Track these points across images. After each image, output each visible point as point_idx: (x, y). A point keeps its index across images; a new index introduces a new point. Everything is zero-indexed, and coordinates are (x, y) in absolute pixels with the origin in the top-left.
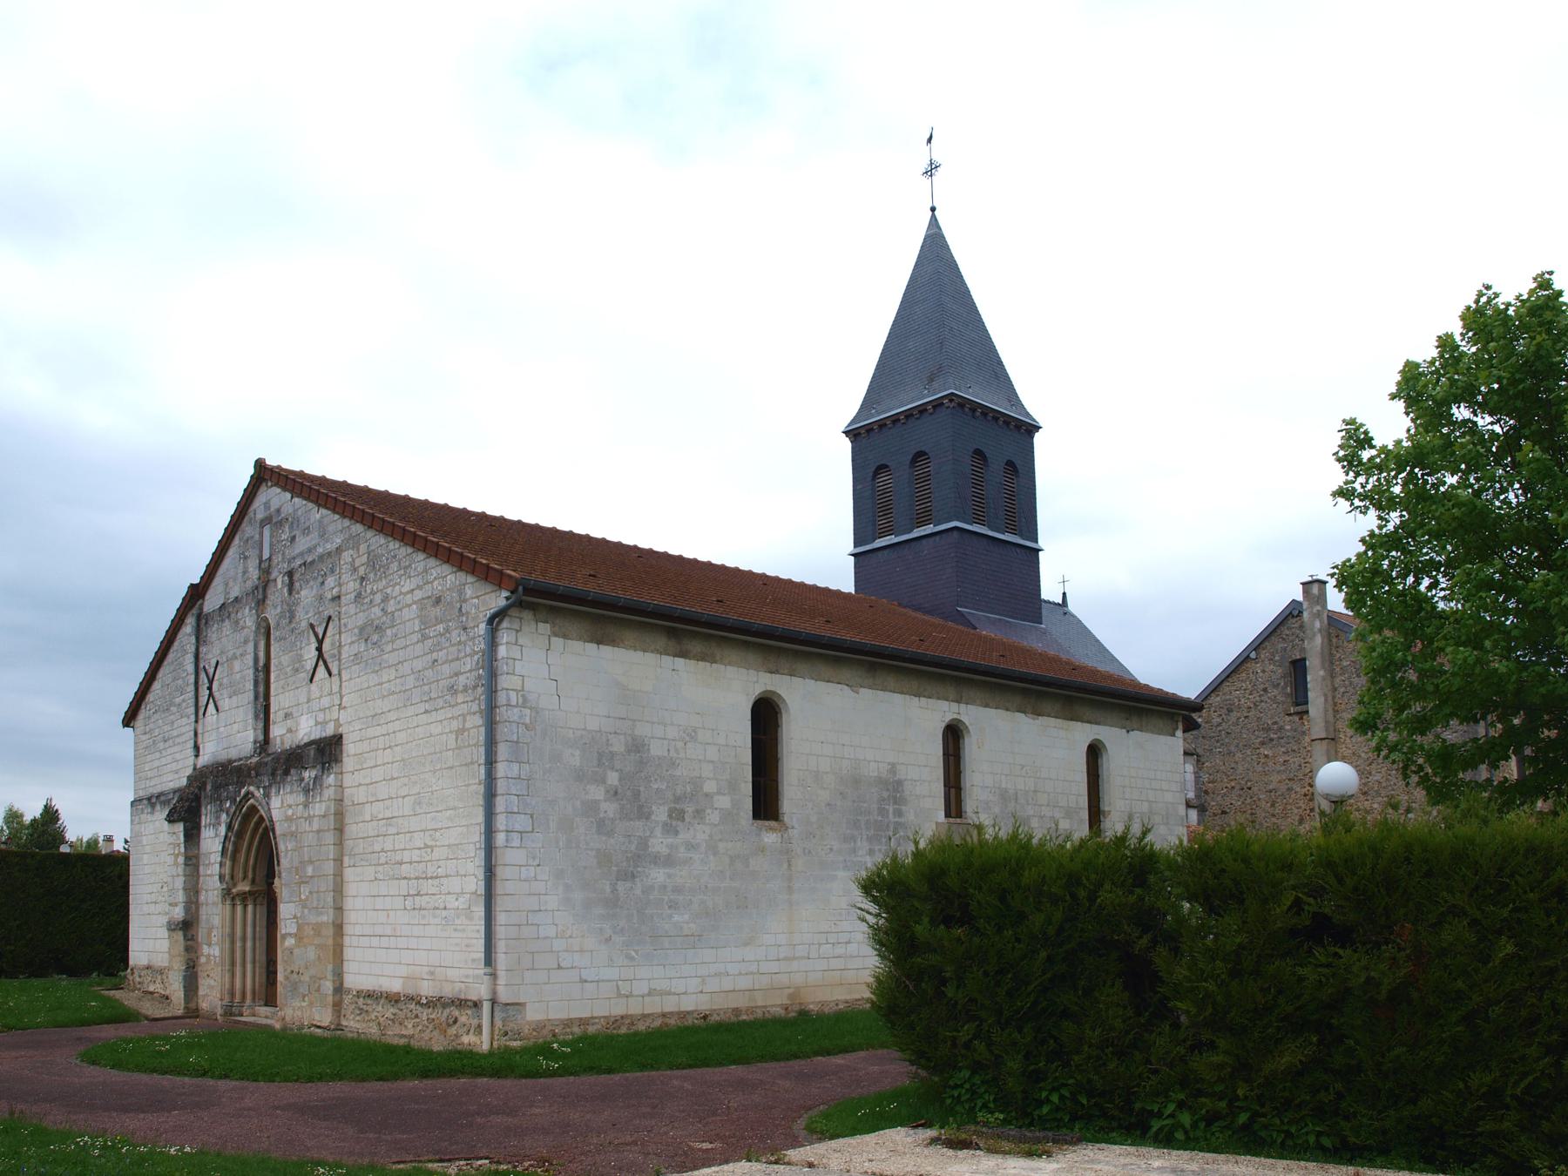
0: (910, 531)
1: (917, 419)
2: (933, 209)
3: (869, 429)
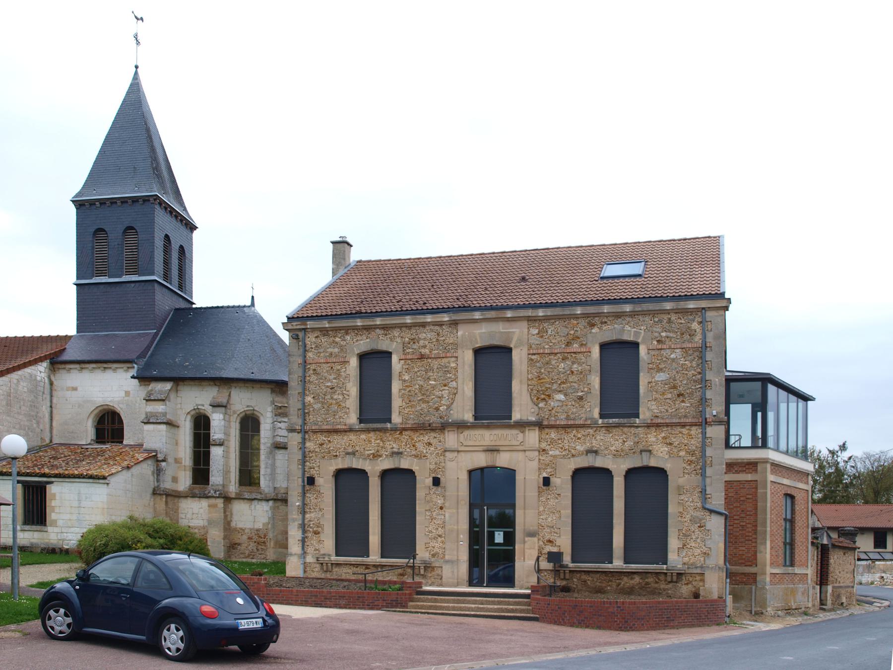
0: (120, 276)
1: (109, 206)
2: (137, 67)
3: (92, 203)
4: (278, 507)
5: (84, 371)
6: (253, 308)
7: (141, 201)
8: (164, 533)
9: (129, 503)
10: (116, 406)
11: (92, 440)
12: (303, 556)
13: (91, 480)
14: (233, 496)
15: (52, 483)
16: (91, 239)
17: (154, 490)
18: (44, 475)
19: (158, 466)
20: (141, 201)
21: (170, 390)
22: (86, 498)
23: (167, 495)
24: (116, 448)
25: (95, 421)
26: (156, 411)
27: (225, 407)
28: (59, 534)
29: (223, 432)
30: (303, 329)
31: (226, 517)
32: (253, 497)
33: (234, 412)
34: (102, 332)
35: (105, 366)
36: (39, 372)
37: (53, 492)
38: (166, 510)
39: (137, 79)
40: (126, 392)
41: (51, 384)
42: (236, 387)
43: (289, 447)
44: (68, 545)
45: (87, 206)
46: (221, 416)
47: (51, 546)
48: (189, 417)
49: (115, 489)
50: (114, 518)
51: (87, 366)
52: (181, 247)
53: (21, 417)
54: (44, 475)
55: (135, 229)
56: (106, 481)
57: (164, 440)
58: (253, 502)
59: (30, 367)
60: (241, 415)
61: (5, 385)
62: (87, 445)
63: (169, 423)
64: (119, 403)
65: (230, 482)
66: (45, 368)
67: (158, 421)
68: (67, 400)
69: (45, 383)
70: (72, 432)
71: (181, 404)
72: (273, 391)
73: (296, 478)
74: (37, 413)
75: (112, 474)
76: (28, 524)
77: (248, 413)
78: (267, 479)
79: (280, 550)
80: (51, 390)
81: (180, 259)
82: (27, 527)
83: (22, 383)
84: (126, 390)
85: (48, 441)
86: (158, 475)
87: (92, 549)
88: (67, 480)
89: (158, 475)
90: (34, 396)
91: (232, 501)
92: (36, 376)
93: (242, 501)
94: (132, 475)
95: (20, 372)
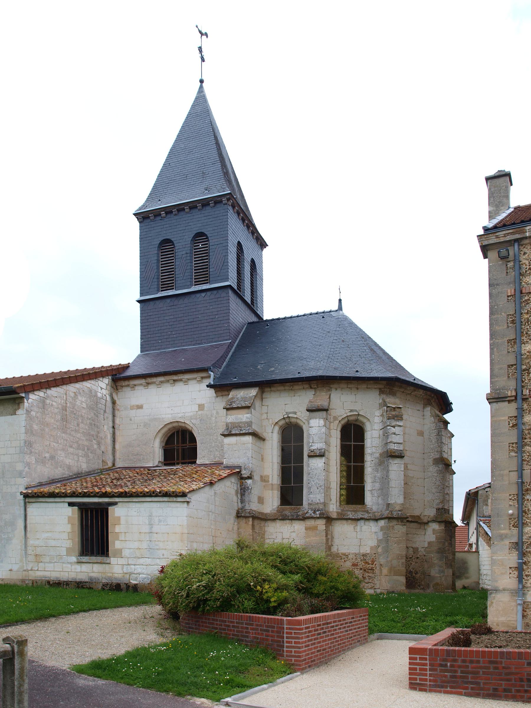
0: (189, 287)
1: (175, 215)
2: (202, 81)
3: (157, 213)
4: (393, 527)
5: (150, 386)
6: (341, 312)
7: (212, 204)
8: (296, 566)
9: (212, 527)
10: (187, 422)
11: (159, 462)
12: (521, 592)
13: (166, 499)
14: (334, 516)
15: (115, 504)
16: (156, 252)
17: (238, 512)
18: (105, 495)
19: (242, 484)
20: (212, 204)
21: (255, 396)
22: (160, 521)
23: (254, 518)
24: (189, 468)
25: (163, 441)
26: (239, 421)
27: (326, 410)
28: (125, 567)
29: (324, 440)
30: (516, 240)
31: (327, 540)
32: (359, 517)
33: (335, 418)
34: (169, 348)
35: (175, 377)
36: (100, 389)
37: (117, 515)
38: (253, 535)
39: (202, 92)
40: (199, 405)
41: (114, 403)
42: (336, 389)
43: (407, 454)
44: (136, 580)
45: (151, 218)
46: (322, 422)
47: (115, 582)
48: (277, 428)
49: (197, 510)
50: (195, 546)
51: (154, 380)
52: (253, 261)
53: (79, 435)
54: (105, 495)
55: (205, 235)
56: (187, 499)
57: (249, 454)
58: (359, 522)
59: (90, 381)
60: (343, 422)
61: (60, 397)
62: (154, 467)
63: (254, 435)
64: (191, 418)
65: (331, 500)
66: (107, 385)
67: (242, 432)
68: (131, 420)
69: (106, 401)
70: (138, 454)
71: (267, 413)
72: (381, 392)
73: (506, 472)
74: (98, 432)
75: (194, 490)
76: (86, 555)
77: (351, 418)
78: (376, 495)
79: (395, 577)
80: (114, 409)
81: (252, 275)
82: (85, 559)
83: (80, 398)
84: (200, 403)
85: (110, 464)
86: (242, 495)
87: (184, 593)
88: (135, 499)
89: (242, 495)
90: (95, 414)
91: (333, 522)
92: (96, 392)
93: (344, 522)
94: (215, 493)
95: (78, 385)
